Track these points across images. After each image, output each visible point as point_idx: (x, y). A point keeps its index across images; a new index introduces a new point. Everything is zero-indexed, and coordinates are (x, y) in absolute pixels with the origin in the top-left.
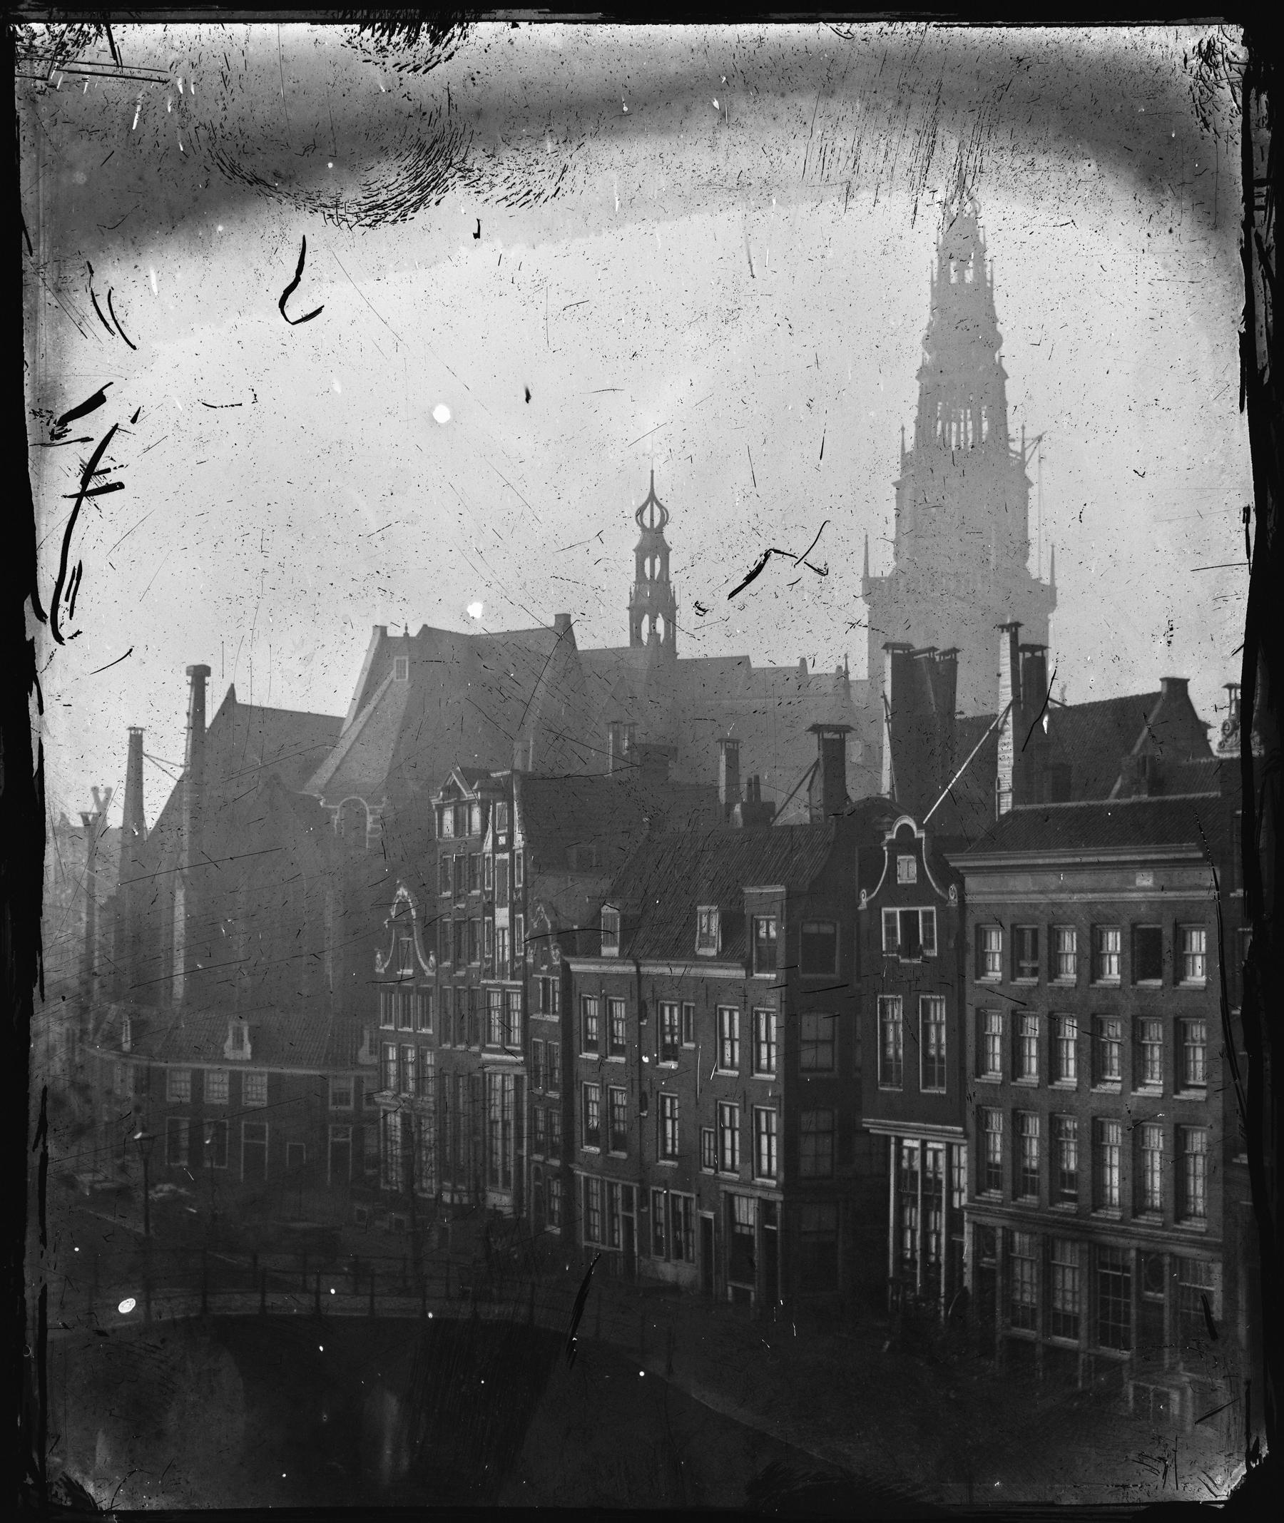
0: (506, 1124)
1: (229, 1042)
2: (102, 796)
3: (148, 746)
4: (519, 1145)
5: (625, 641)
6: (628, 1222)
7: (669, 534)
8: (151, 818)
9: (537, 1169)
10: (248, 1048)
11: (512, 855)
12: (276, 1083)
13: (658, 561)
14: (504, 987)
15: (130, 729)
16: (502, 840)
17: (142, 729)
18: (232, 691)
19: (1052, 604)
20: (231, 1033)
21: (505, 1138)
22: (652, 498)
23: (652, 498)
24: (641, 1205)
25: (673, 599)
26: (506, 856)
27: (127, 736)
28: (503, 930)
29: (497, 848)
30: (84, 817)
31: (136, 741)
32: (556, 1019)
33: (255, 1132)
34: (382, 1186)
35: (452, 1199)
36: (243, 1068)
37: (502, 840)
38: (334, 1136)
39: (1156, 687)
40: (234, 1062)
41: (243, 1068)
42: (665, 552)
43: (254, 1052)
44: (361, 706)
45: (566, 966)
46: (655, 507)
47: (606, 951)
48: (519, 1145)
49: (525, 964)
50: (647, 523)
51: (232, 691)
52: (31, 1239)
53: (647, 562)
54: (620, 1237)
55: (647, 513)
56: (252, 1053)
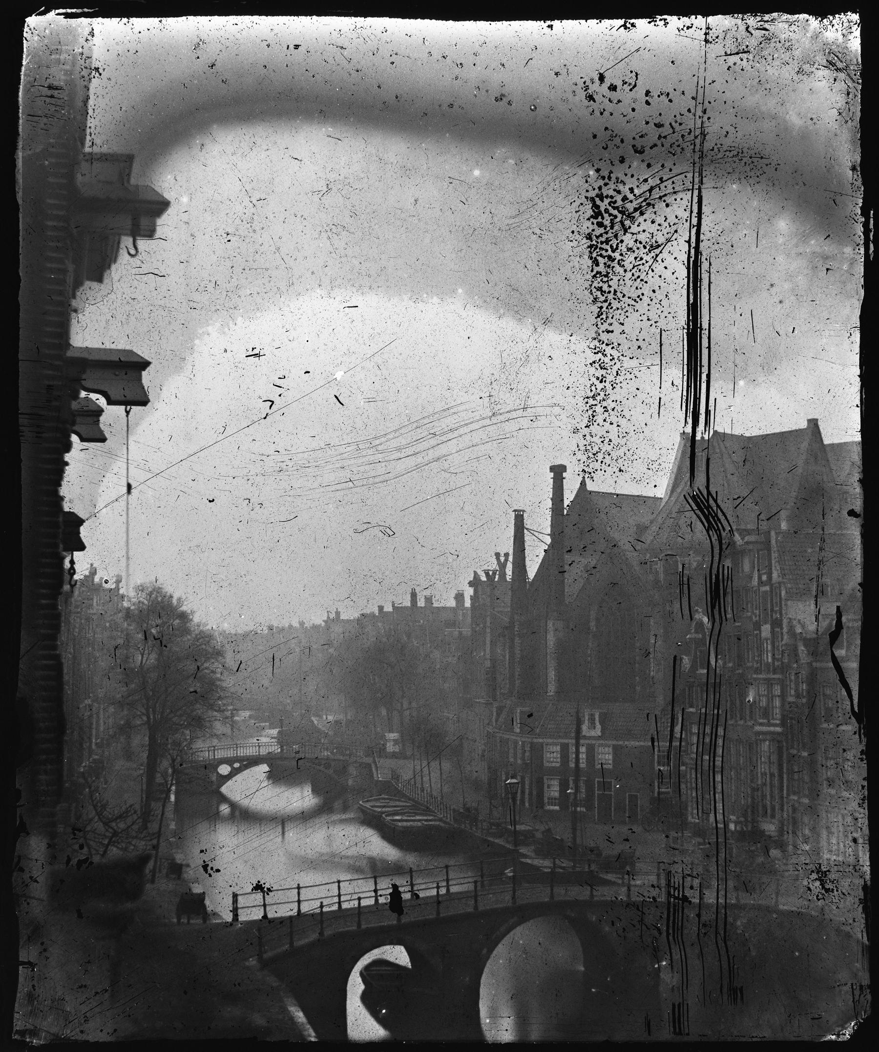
2: (502, 559)
3: (528, 523)
4: (781, 789)
8: (532, 570)
12: (617, 751)
15: (515, 511)
16: (764, 578)
17: (524, 511)
20: (587, 718)
26: (767, 588)
28: (767, 639)
29: (761, 583)
30: (487, 573)
31: (519, 518)
33: (605, 786)
34: (690, 818)
35: (735, 828)
37: (764, 578)
39: (804, 425)
40: (590, 738)
44: (672, 491)
49: (782, 663)
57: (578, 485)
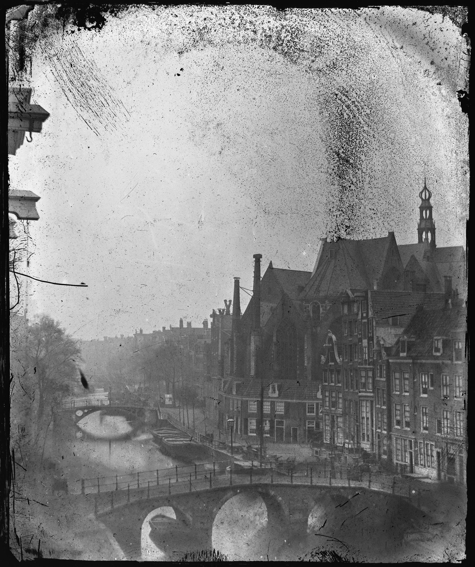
0: (367, 418)
1: (270, 391)
2: (228, 303)
4: (372, 426)
5: (416, 241)
6: (411, 453)
7: (432, 201)
8: (243, 309)
9: (379, 435)
10: (277, 392)
11: (368, 320)
13: (428, 212)
14: (366, 368)
15: (235, 278)
16: (365, 315)
17: (239, 278)
18: (271, 263)
19: (278, 9)
21: (367, 424)
22: (425, 188)
23: (425, 188)
24: (415, 448)
25: (434, 225)
26: (365, 321)
27: (234, 280)
28: (365, 347)
29: (363, 318)
32: (384, 379)
36: (275, 400)
37: (365, 315)
38: (308, 425)
40: (272, 398)
41: (275, 400)
42: (430, 208)
43: (279, 394)
45: (388, 360)
46: (427, 191)
47: (401, 355)
48: (372, 426)
50: (424, 197)
51: (271, 263)
52: (467, 401)
53: (424, 212)
54: (408, 460)
55: (424, 193)
56: (279, 394)
57: (268, 265)
